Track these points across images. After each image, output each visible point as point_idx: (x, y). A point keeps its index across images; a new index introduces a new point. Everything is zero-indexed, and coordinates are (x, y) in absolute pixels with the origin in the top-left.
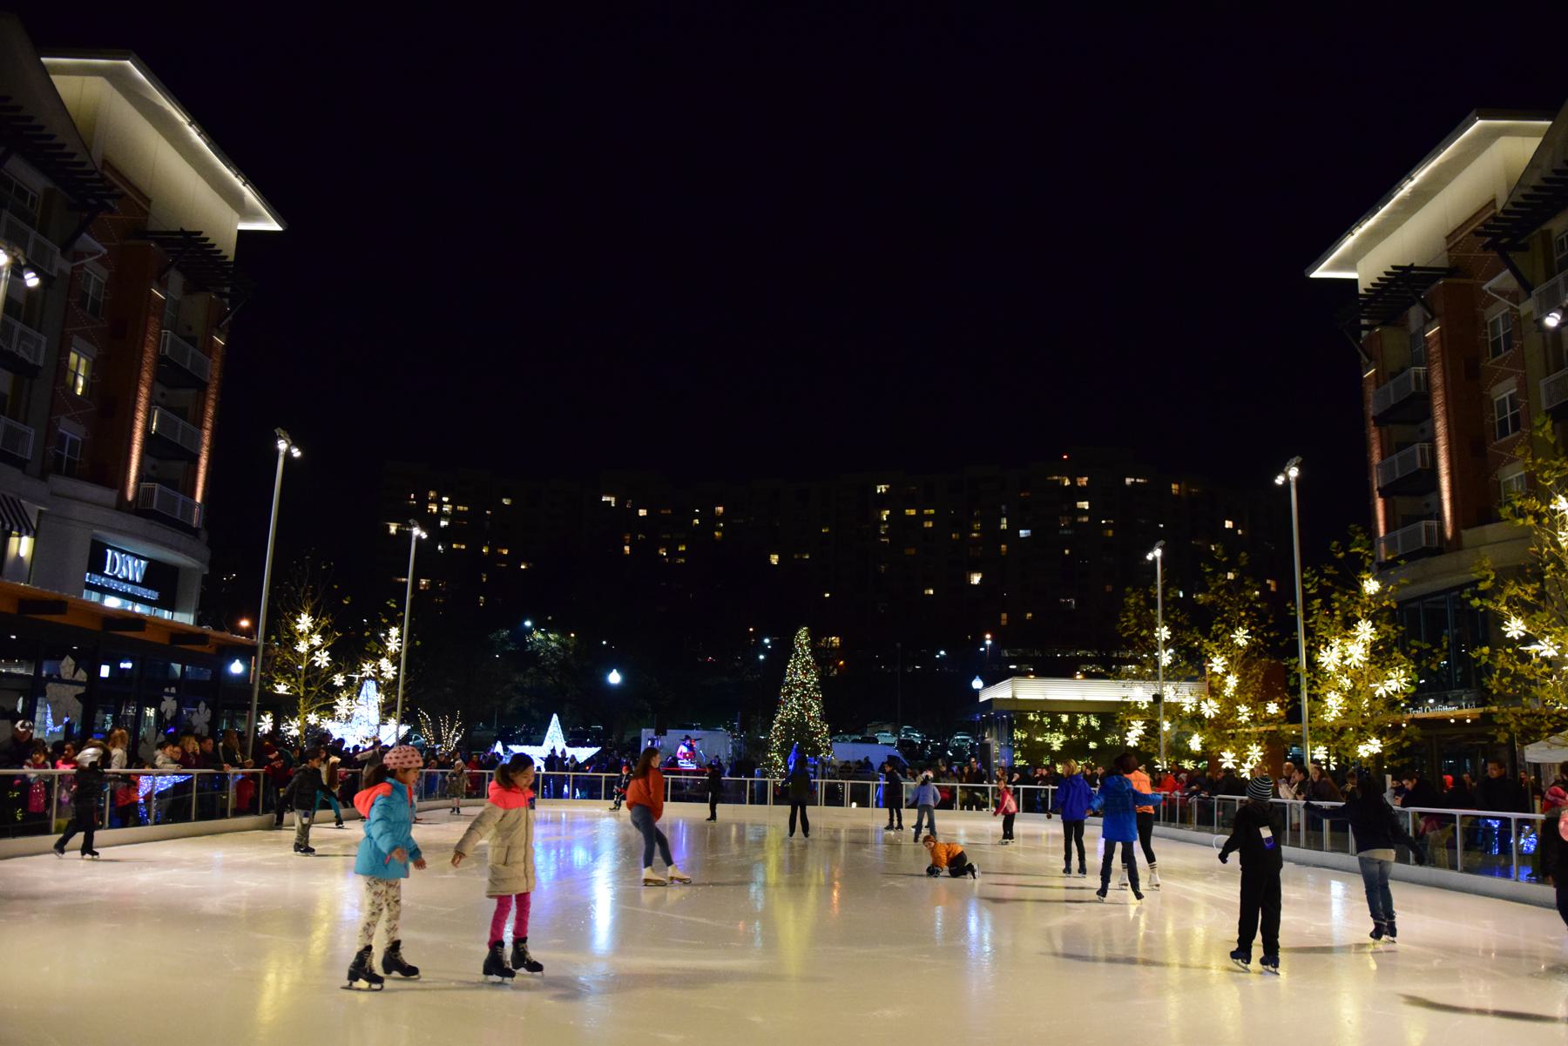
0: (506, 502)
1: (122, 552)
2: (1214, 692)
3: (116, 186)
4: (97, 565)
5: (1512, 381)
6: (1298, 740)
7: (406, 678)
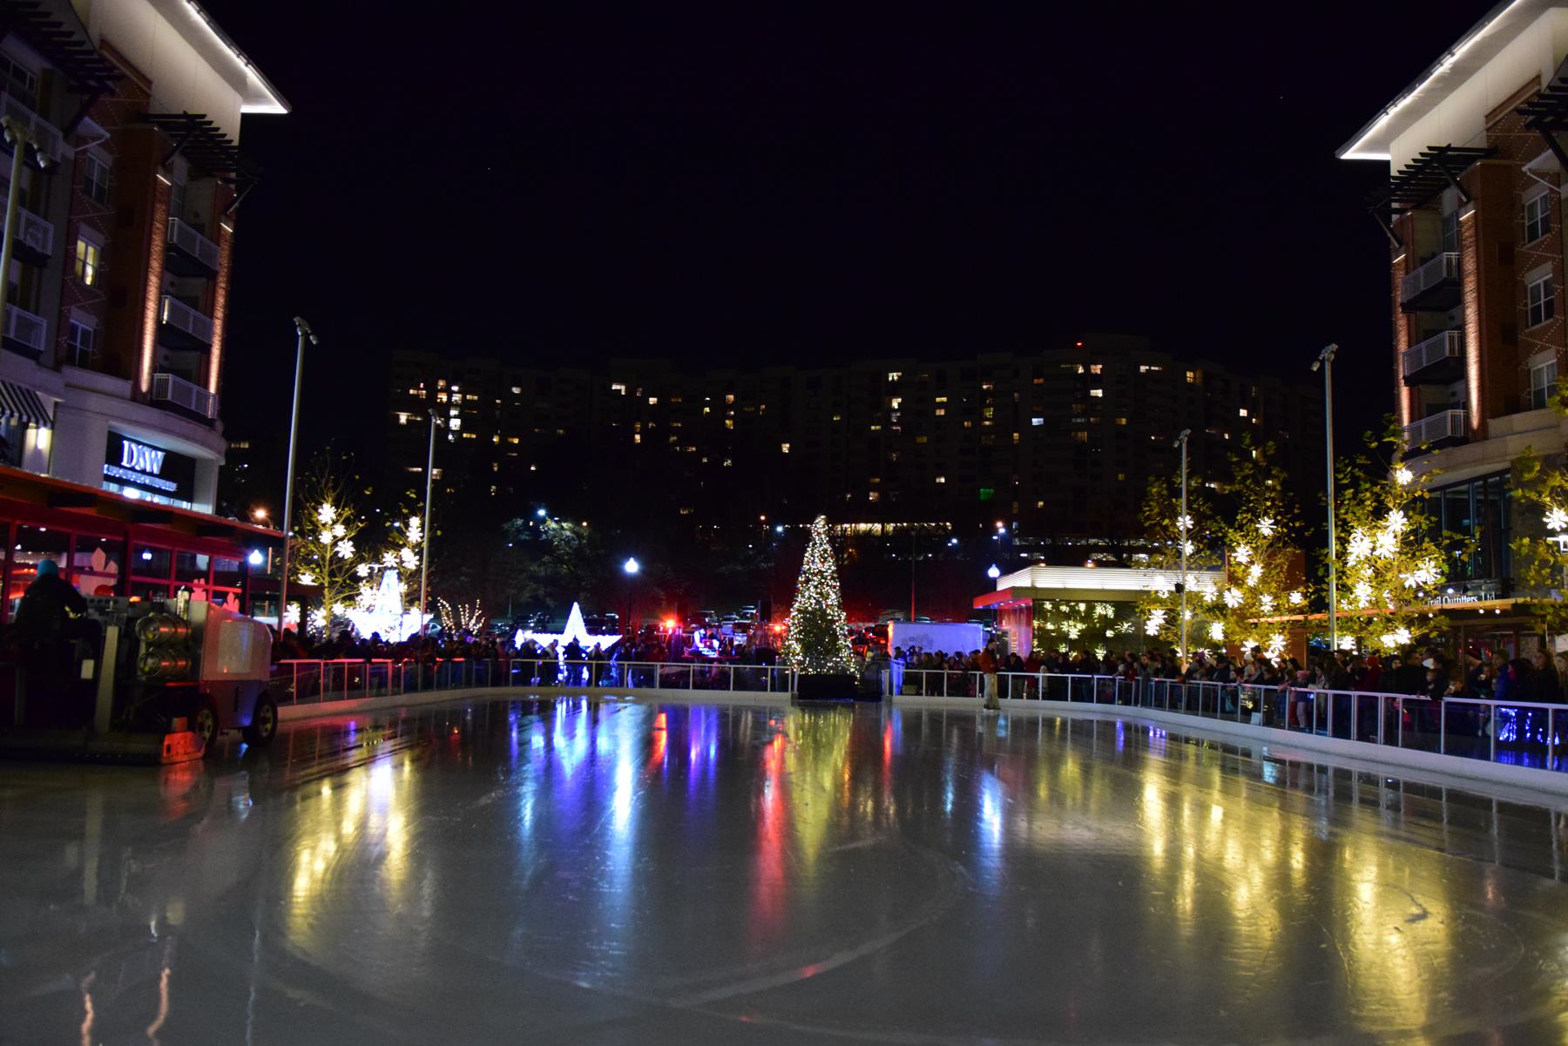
0: (516, 390)
1: (139, 443)
2: (1235, 580)
3: (115, 68)
4: (114, 456)
5: (1549, 266)
6: (1323, 628)
7: (429, 567)
